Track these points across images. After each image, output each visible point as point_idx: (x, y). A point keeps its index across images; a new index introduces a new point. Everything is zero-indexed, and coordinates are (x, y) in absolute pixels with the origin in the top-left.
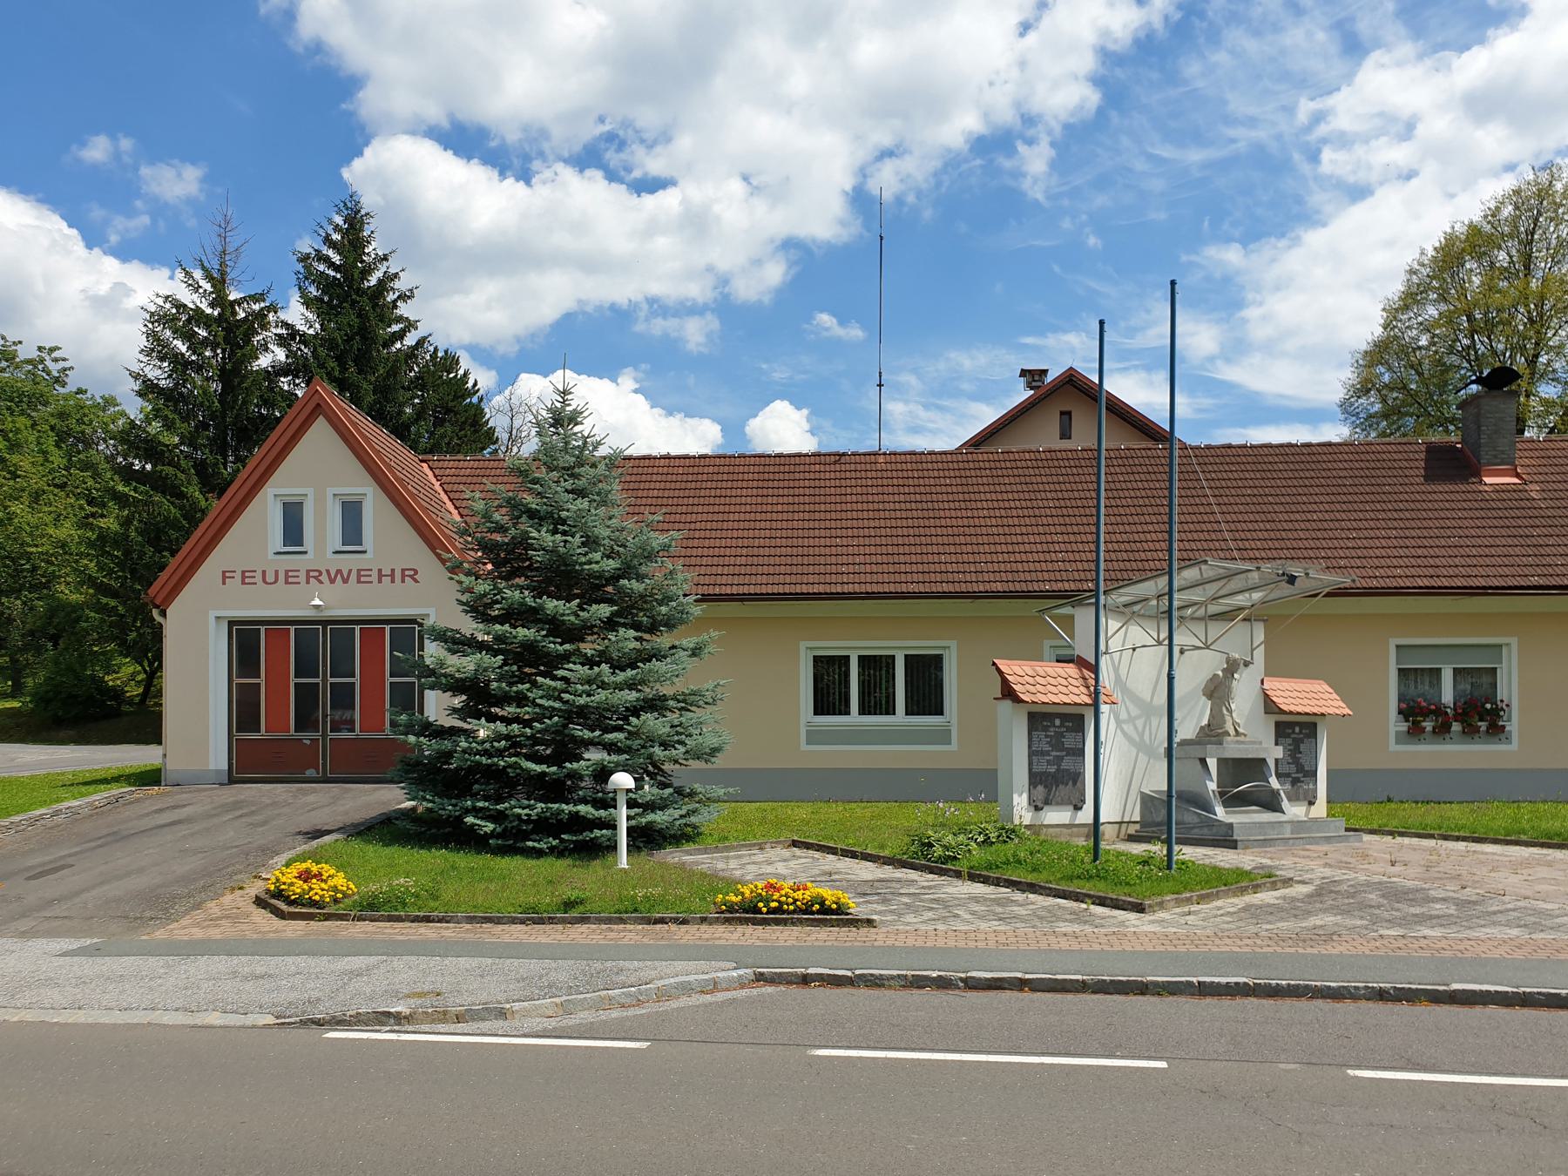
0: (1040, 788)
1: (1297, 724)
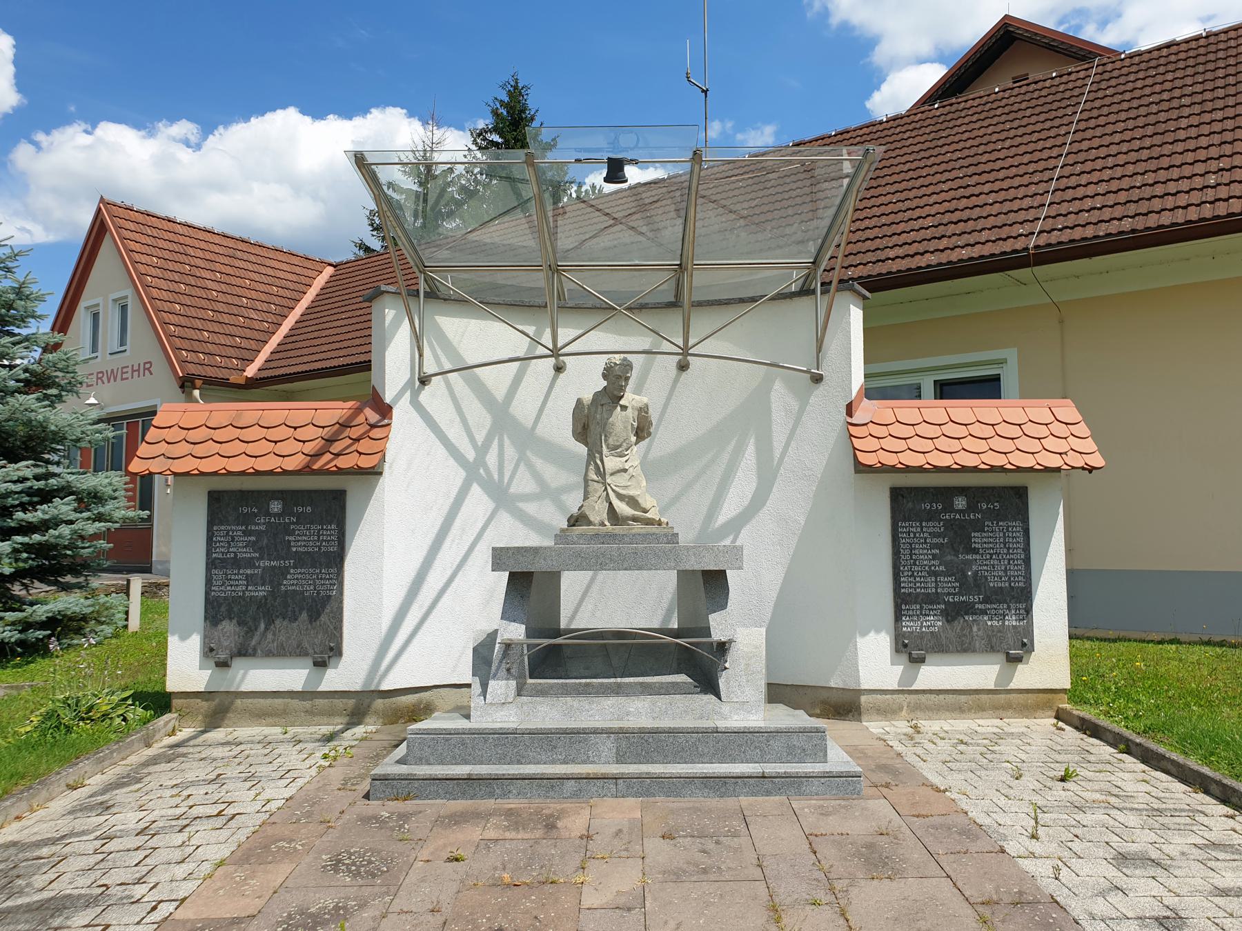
0: (228, 627)
1: (962, 491)
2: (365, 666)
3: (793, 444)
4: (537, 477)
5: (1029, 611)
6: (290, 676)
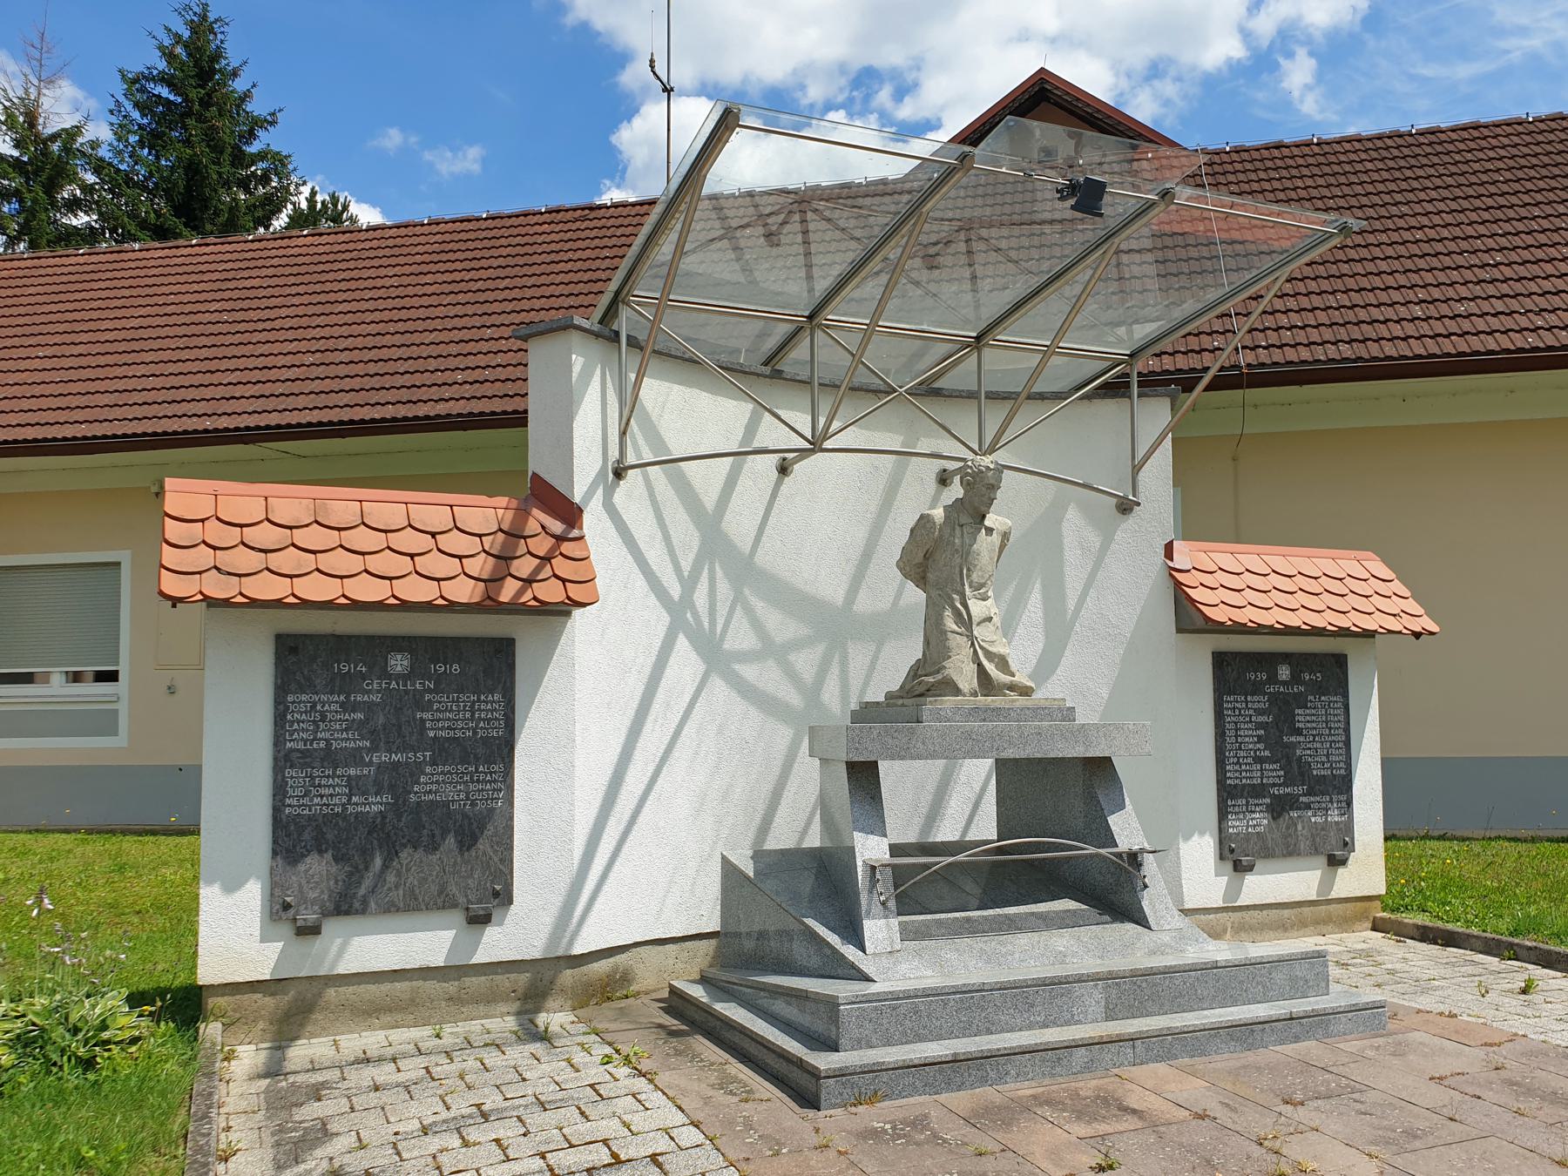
1: (1286, 657)
2: (547, 920)
3: (1092, 593)
4: (757, 625)
5: (1349, 803)
6: (424, 943)
